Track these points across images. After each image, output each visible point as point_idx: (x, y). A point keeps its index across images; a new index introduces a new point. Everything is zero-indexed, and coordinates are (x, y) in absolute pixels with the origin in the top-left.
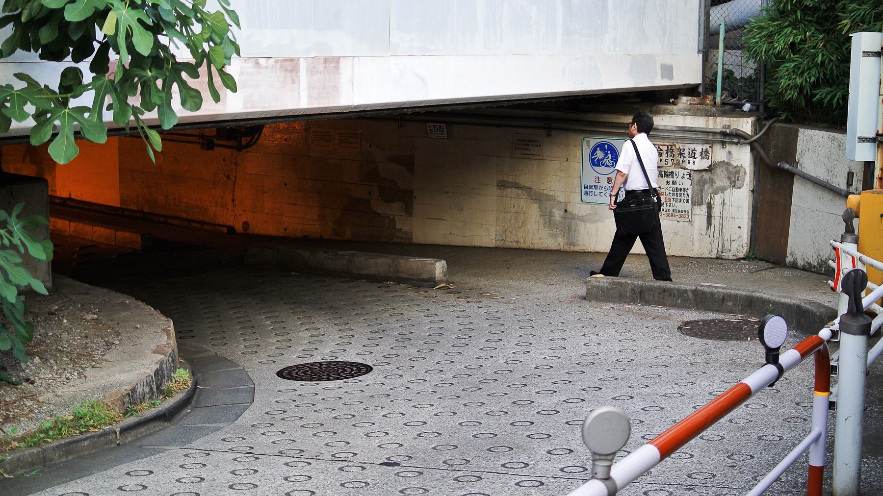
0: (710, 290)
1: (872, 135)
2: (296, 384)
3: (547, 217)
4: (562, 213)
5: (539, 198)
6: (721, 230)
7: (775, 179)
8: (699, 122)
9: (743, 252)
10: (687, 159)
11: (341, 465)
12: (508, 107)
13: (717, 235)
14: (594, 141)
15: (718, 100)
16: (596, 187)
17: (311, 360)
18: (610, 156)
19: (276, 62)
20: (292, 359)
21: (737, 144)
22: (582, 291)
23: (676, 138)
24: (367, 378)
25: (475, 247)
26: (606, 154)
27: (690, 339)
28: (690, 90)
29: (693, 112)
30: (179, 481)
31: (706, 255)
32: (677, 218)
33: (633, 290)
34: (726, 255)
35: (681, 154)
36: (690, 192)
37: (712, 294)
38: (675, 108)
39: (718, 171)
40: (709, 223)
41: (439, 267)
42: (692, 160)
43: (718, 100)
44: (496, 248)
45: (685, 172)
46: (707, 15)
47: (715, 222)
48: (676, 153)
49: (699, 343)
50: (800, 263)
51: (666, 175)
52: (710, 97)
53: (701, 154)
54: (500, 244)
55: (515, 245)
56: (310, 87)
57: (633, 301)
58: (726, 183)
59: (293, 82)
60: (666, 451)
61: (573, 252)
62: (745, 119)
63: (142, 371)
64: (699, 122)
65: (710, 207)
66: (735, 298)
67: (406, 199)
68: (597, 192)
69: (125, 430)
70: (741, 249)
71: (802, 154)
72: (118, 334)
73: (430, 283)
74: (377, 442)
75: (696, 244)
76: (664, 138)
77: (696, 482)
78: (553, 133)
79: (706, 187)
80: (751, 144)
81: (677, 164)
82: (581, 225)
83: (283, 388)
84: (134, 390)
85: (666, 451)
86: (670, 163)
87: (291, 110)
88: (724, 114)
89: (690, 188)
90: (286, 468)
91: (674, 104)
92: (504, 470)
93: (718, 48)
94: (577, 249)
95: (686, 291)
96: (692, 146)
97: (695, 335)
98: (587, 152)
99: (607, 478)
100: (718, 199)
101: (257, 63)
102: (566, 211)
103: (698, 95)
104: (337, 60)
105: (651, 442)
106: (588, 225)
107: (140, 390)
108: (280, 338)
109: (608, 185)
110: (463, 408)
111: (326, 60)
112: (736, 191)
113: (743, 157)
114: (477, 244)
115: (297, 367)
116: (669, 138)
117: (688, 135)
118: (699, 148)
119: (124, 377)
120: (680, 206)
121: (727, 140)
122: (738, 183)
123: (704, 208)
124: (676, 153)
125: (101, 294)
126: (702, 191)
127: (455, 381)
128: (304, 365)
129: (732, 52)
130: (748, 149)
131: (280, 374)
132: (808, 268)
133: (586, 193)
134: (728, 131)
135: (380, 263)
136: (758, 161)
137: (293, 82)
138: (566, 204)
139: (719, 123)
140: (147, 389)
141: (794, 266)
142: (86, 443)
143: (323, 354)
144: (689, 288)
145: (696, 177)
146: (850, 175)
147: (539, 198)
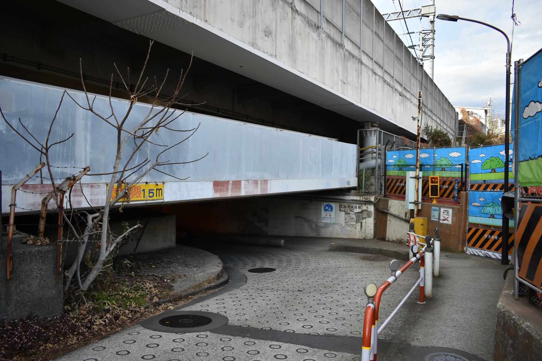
1: (413, 201)
7: (382, 215)
8: (358, 198)
9: (372, 237)
14: (325, 204)
24: (276, 272)
25: (288, 236)
28: (354, 188)
40: (361, 228)
41: (282, 241)
47: (363, 228)
54: (296, 235)
56: (261, 188)
57: (344, 251)
58: (366, 216)
64: (358, 198)
65: (361, 223)
81: (351, 211)
82: (321, 229)
90: (151, 339)
100: (364, 221)
111: (265, 181)
113: (371, 208)
118: (358, 206)
120: (352, 223)
123: (360, 224)
131: (249, 271)
132: (393, 242)
136: (376, 209)
141: (389, 241)
143: (258, 265)
145: (357, 214)
146: (406, 213)
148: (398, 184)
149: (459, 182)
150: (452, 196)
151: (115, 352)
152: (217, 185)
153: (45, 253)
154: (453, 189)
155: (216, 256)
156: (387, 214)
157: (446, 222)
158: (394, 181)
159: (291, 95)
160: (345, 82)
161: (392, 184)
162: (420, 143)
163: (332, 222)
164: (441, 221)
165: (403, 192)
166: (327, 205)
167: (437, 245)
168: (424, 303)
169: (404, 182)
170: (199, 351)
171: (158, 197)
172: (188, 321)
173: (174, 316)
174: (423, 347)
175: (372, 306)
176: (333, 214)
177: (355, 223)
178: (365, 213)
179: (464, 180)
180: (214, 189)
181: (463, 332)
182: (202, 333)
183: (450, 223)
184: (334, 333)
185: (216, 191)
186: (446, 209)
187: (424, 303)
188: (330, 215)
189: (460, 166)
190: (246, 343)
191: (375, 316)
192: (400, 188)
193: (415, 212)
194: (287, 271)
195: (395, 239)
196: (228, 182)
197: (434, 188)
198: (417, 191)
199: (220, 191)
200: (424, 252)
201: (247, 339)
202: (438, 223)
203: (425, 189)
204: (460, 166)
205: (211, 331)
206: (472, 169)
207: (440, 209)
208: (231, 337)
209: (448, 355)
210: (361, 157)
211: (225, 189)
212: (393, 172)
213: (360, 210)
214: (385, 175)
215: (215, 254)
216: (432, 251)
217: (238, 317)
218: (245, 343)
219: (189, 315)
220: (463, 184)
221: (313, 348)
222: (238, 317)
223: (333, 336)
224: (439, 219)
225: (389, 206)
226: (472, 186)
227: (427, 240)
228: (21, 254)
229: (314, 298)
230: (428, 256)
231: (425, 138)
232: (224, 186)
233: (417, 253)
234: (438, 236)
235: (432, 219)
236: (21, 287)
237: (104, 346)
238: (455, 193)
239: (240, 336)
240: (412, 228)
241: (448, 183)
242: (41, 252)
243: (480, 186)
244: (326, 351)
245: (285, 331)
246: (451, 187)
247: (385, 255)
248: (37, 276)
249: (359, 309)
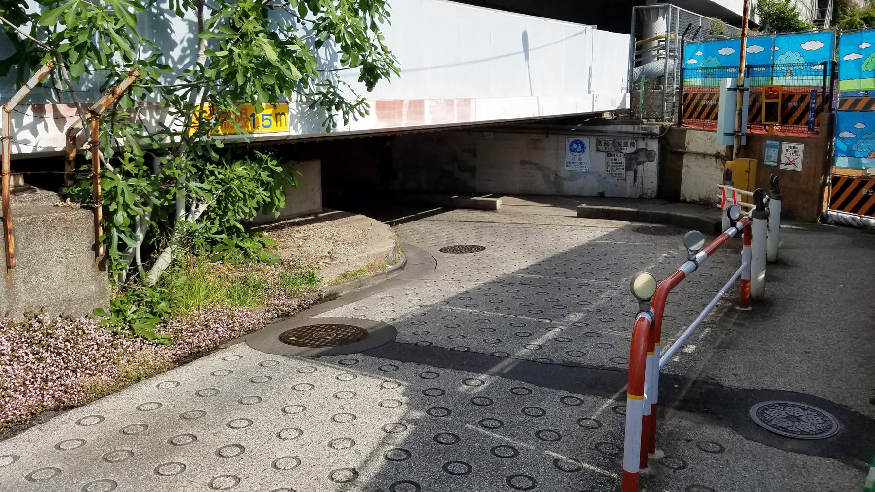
35: (619, 145)
39: (641, 153)
47: (639, 180)
50: (688, 200)
58: (644, 159)
65: (636, 172)
71: (689, 143)
80: (659, 139)
81: (617, 150)
82: (565, 182)
90: (17, 452)
98: (568, 145)
99: (694, 261)
100: (640, 167)
111: (465, 100)
113: (654, 146)
119: (381, 250)
120: (618, 172)
123: (633, 172)
132: (693, 202)
136: (662, 148)
141: (685, 201)
148: (703, 102)
149: (817, 96)
150: (804, 121)
151: (194, 392)
153: (71, 221)
154: (807, 109)
156: (683, 153)
157: (791, 167)
158: (698, 97)
161: (694, 103)
162: (747, 28)
163: (584, 170)
164: (782, 167)
165: (713, 116)
167: (774, 206)
168: (750, 308)
169: (715, 97)
170: (340, 389)
171: (282, 129)
173: (303, 328)
174: (745, 390)
175: (647, 317)
176: (585, 157)
178: (642, 154)
179: (828, 90)
181: (821, 363)
182: (349, 356)
183: (799, 168)
184: (579, 359)
185: (381, 117)
186: (793, 145)
187: (750, 308)
188: (580, 159)
189: (822, 67)
190: (423, 375)
191: (654, 335)
192: (707, 110)
193: (735, 151)
194: (505, 252)
195: (696, 198)
196: (402, 101)
197: (771, 107)
198: (740, 114)
200: (751, 219)
201: (426, 368)
202: (776, 169)
203: (755, 110)
204: (822, 67)
205: (365, 352)
206: (843, 71)
207: (781, 145)
208: (398, 363)
209: (786, 405)
210: (639, 56)
212: (694, 82)
213: (633, 150)
214: (681, 87)
216: (766, 217)
217: (413, 329)
218: (420, 376)
220: (827, 96)
221: (540, 386)
222: (413, 329)
223: (578, 366)
224: (779, 162)
225: (687, 140)
226: (842, 102)
227: (757, 198)
228: (28, 223)
229: (548, 297)
230: (757, 226)
231: (757, 20)
233: (737, 220)
234: (777, 192)
235: (766, 162)
236: (33, 280)
237: (176, 380)
238: (810, 116)
239: (413, 361)
240: (728, 177)
241: (796, 98)
242: (65, 221)
243: (857, 101)
244: (565, 393)
245: (492, 355)
246: (803, 106)
247: (678, 226)
248: (60, 262)
249: (628, 318)
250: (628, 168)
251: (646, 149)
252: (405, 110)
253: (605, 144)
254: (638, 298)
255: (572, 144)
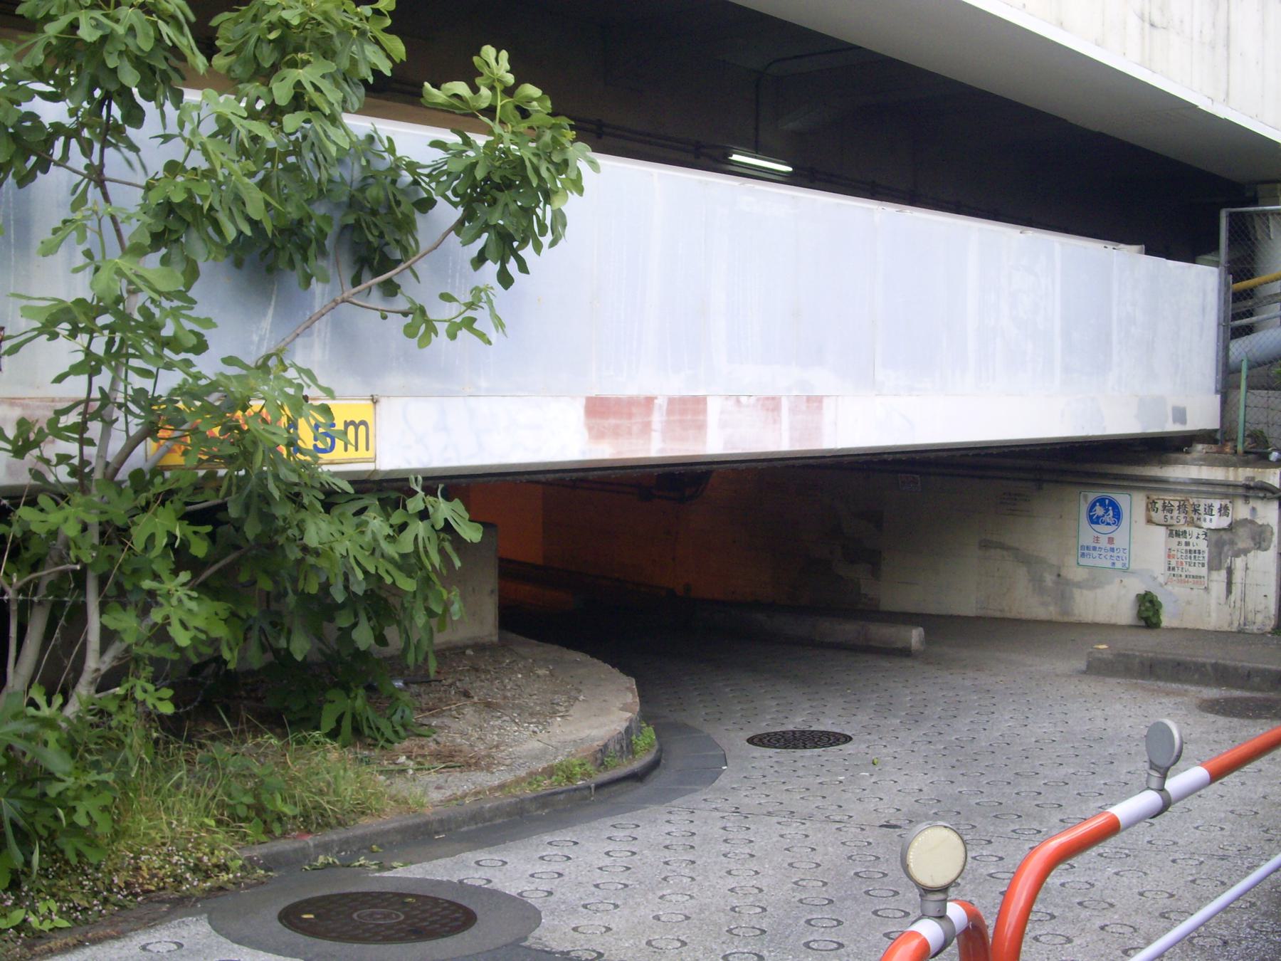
0: (1233, 663)
2: (771, 752)
3: (1037, 582)
4: (1054, 578)
5: (1027, 560)
6: (1243, 600)
8: (1217, 474)
10: (1203, 516)
11: (838, 825)
12: (998, 455)
13: (1238, 605)
14: (1093, 495)
15: (1240, 448)
16: (1094, 549)
17: (783, 729)
18: (1111, 512)
19: (758, 400)
20: (764, 726)
21: (1262, 498)
22: (1082, 665)
23: (1191, 492)
24: (848, 748)
26: (1107, 510)
27: (1211, 717)
29: (1209, 462)
30: (669, 834)
31: (1226, 628)
32: (1190, 585)
33: (1142, 663)
34: (1249, 628)
35: (1195, 511)
36: (1206, 555)
37: (1236, 669)
38: (1188, 457)
40: (1229, 591)
41: (916, 636)
42: (1208, 517)
43: (1240, 448)
44: (978, 618)
45: (1201, 531)
46: (1226, 349)
47: (1237, 590)
48: (1189, 509)
49: (1222, 721)
51: (1178, 534)
52: (1230, 444)
53: (1220, 510)
54: (981, 613)
55: (998, 615)
57: (1142, 676)
58: (1249, 543)
59: (775, 422)
60: (1217, 775)
61: (1066, 623)
62: (1272, 470)
63: (613, 727)
64: (1217, 474)
65: (1230, 572)
66: (1263, 673)
67: (873, 560)
68: (1095, 553)
69: (600, 786)
70: (1267, 622)
72: (580, 691)
73: (906, 653)
74: (872, 807)
75: (1214, 615)
76: (1175, 491)
77: (1230, 853)
78: (1045, 486)
79: (1226, 548)
81: (1192, 523)
82: (1077, 592)
83: (755, 754)
84: (606, 746)
85: (1217, 775)
86: (1183, 521)
87: (772, 453)
88: (1246, 464)
89: (1206, 550)
91: (1187, 452)
92: (1015, 836)
93: (1238, 387)
94: (1072, 619)
95: (1204, 665)
96: (1209, 502)
97: (1217, 713)
99: (1161, 790)
100: (1239, 563)
101: (738, 402)
102: (1059, 575)
103: (1215, 442)
104: (819, 399)
105: (1202, 764)
106: (1085, 592)
107: (611, 747)
108: (745, 707)
109: (1109, 546)
110: (961, 778)
111: (809, 399)
112: (1261, 554)
114: (955, 612)
115: (768, 734)
116: (1181, 491)
117: (1204, 488)
118: (1217, 504)
119: (594, 733)
120: (1194, 571)
121: (1251, 493)
122: (1264, 545)
123: (1223, 573)
124: (1189, 509)
125: (554, 651)
126: (1220, 554)
127: (947, 752)
128: (776, 733)
129: (1256, 392)
130: (1275, 505)
131: (751, 741)
133: (1083, 555)
134: (1252, 484)
135: (848, 630)
137: (775, 422)
138: (1059, 568)
139: (1242, 475)
140: (618, 747)
142: (562, 797)
143: (796, 722)
144: (1208, 661)
145: (1214, 537)
147: (1027, 560)
152: (599, 410)
155: (632, 682)
159: (962, 85)
160: (1157, 19)
166: (1101, 501)
171: (346, 456)
172: (386, 916)
177: (1204, 571)
178: (1243, 531)
180: (590, 429)
185: (597, 434)
188: (1111, 540)
196: (649, 401)
199: (616, 433)
210: (1240, 313)
211: (635, 429)
213: (1224, 522)
215: (627, 670)
219: (402, 896)
232: (630, 416)
250: (1214, 565)
251: (1252, 522)
252: (657, 418)
253: (1164, 507)
254: (918, 884)
255: (1093, 505)
